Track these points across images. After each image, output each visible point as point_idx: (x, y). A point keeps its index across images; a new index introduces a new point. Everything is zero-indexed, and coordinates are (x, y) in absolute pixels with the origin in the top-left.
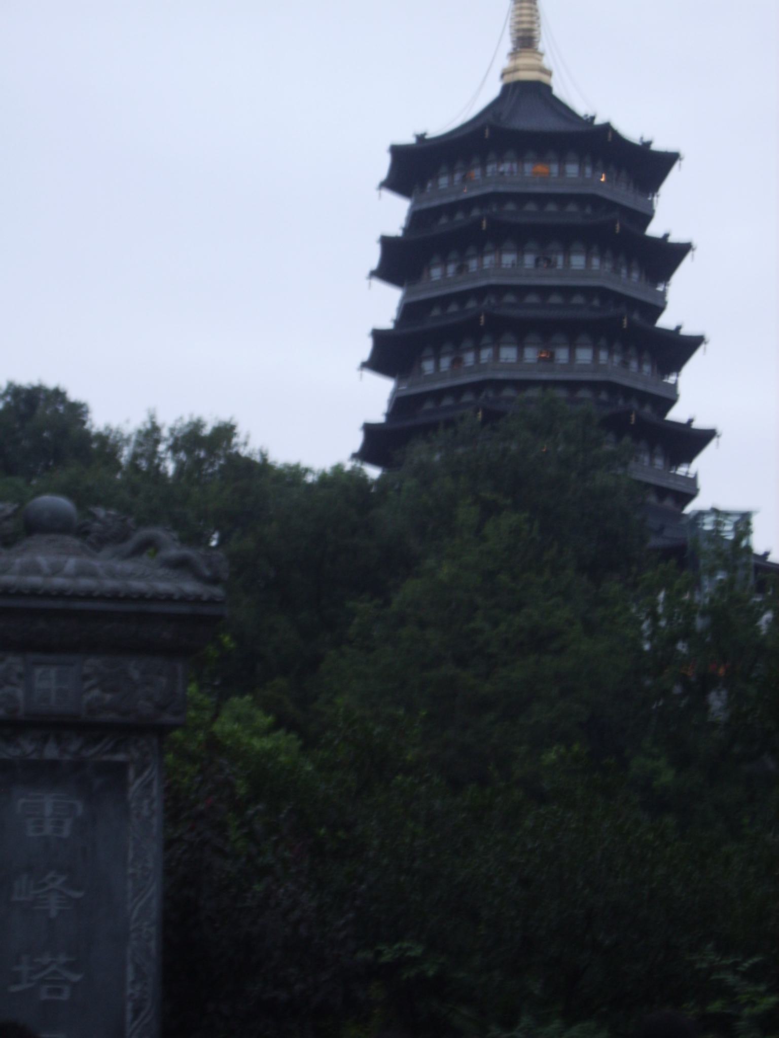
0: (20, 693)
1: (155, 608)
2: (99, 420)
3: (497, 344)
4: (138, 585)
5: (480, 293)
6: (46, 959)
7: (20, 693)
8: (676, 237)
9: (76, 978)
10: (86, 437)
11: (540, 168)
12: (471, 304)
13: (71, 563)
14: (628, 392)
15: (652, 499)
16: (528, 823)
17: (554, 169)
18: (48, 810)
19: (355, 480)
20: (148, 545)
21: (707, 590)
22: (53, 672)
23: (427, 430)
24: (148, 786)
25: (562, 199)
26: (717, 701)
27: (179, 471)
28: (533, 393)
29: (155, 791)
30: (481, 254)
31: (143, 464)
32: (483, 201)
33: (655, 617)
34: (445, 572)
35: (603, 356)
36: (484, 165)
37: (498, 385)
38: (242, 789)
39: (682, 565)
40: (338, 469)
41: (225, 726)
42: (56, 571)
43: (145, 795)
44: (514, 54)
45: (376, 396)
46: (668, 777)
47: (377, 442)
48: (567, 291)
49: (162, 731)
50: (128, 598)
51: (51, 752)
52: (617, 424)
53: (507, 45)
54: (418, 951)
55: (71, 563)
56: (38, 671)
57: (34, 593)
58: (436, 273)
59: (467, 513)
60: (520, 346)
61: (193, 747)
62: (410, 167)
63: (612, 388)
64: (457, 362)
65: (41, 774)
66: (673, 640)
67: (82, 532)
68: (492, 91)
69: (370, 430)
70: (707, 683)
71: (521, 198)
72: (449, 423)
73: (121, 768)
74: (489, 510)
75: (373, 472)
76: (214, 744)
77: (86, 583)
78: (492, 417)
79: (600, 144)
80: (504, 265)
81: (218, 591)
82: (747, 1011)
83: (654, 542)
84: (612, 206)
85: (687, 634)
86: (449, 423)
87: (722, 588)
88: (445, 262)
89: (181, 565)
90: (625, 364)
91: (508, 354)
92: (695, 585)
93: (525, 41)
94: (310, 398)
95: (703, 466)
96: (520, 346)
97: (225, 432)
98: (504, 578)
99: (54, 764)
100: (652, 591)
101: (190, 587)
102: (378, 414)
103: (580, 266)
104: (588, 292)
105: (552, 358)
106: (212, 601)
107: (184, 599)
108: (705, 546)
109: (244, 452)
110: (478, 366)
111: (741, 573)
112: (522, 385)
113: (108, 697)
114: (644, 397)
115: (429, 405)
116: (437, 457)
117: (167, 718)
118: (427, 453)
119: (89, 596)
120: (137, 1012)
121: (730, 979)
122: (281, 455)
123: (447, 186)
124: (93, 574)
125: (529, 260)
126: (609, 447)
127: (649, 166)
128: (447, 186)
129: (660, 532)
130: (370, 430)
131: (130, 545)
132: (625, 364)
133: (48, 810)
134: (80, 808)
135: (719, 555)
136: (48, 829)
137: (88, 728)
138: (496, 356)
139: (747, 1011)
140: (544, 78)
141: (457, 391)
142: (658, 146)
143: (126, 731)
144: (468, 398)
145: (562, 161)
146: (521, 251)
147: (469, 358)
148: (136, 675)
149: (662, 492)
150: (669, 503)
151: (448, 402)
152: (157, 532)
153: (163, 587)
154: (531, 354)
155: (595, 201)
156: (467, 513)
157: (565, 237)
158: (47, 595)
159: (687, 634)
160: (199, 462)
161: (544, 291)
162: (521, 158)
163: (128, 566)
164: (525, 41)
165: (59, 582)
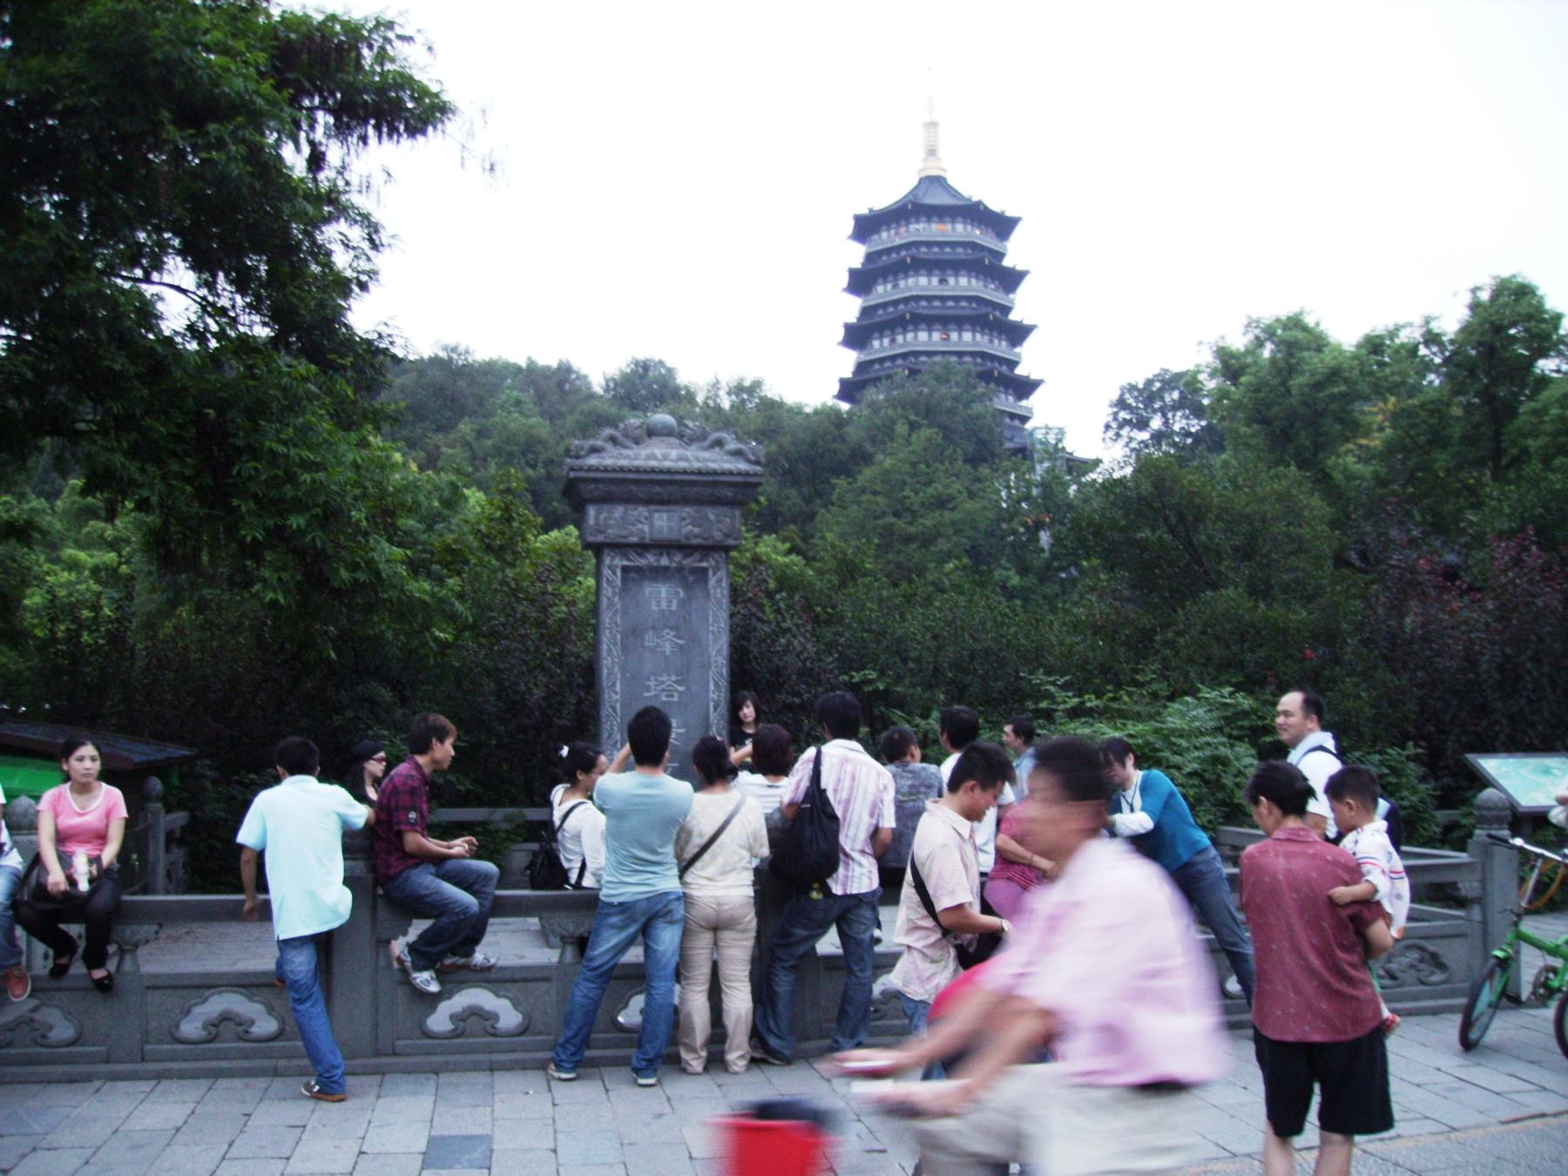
0: (646, 528)
1: (722, 478)
2: (683, 378)
3: (916, 330)
4: (713, 466)
5: (906, 300)
6: (664, 678)
7: (646, 528)
8: (1027, 322)
9: (681, 689)
10: (677, 389)
11: (941, 227)
12: (901, 307)
13: (674, 453)
14: (993, 358)
15: (1007, 420)
16: (937, 604)
17: (949, 226)
18: (664, 594)
19: (837, 412)
20: (719, 443)
21: (1041, 469)
22: (665, 516)
23: (875, 381)
24: (720, 581)
25: (953, 245)
26: (1045, 538)
27: (732, 406)
28: (937, 359)
29: (724, 584)
30: (905, 332)
31: (711, 403)
32: (908, 246)
33: (1008, 487)
34: (888, 462)
35: (978, 336)
36: (908, 223)
37: (916, 354)
38: (772, 585)
39: (1025, 458)
40: (824, 405)
41: (762, 549)
42: (665, 458)
43: (718, 586)
44: (925, 160)
45: (846, 362)
46: (1015, 580)
47: (848, 390)
48: (957, 299)
49: (727, 549)
50: (707, 473)
51: (665, 561)
52: (986, 376)
53: (922, 155)
54: (874, 675)
55: (674, 453)
56: (656, 516)
57: (653, 471)
58: (880, 289)
59: (901, 428)
60: (930, 330)
61: (744, 561)
63: (983, 355)
64: (893, 341)
65: (659, 573)
66: (1019, 502)
67: (681, 436)
69: (843, 382)
70: (1039, 526)
71: (929, 244)
72: (889, 377)
73: (704, 571)
74: (914, 426)
75: (845, 406)
76: (756, 559)
77: (683, 465)
78: (914, 372)
79: (976, 213)
80: (923, 284)
81: (758, 469)
82: (1062, 707)
83: (1008, 445)
84: (983, 248)
85: (1027, 498)
86: (889, 377)
87: (1047, 471)
88: (885, 282)
89: (737, 454)
90: (991, 341)
91: (923, 336)
92: (1032, 469)
93: (932, 152)
94: (809, 372)
95: (1034, 402)
96: (930, 330)
97: (757, 384)
98: (922, 466)
99: (666, 569)
100: (1007, 473)
101: (743, 466)
102: (848, 373)
103: (963, 284)
104: (973, 354)
105: (948, 339)
106: (755, 475)
107: (740, 474)
108: (1038, 446)
109: (769, 395)
110: (908, 288)
111: (1059, 463)
112: (930, 354)
113: (697, 530)
114: (1002, 361)
115: (877, 366)
116: (881, 397)
117: (731, 542)
118: (876, 395)
119: (685, 472)
120: (715, 708)
121: (1052, 688)
122: (790, 399)
123: (887, 238)
124: (687, 460)
125: (935, 280)
126: (980, 390)
128: (887, 238)
129: (1011, 440)
130: (843, 382)
131: (707, 442)
132: (991, 341)
133: (664, 594)
134: (682, 593)
135: (1047, 452)
136: (664, 605)
137: (686, 548)
138: (916, 337)
139: (1062, 707)
141: (893, 358)
142: (1019, 268)
143: (707, 550)
144: (899, 362)
145: (953, 222)
146: (929, 275)
147: (900, 338)
148: (712, 517)
149: (1012, 416)
150: (1017, 422)
151: (888, 364)
152: (723, 435)
153: (727, 466)
155: (973, 246)
156: (901, 428)
157: (957, 266)
158: (661, 472)
159: (1027, 498)
160: (743, 401)
161: (943, 299)
162: (929, 221)
163: (707, 455)
164: (932, 152)
165: (667, 464)
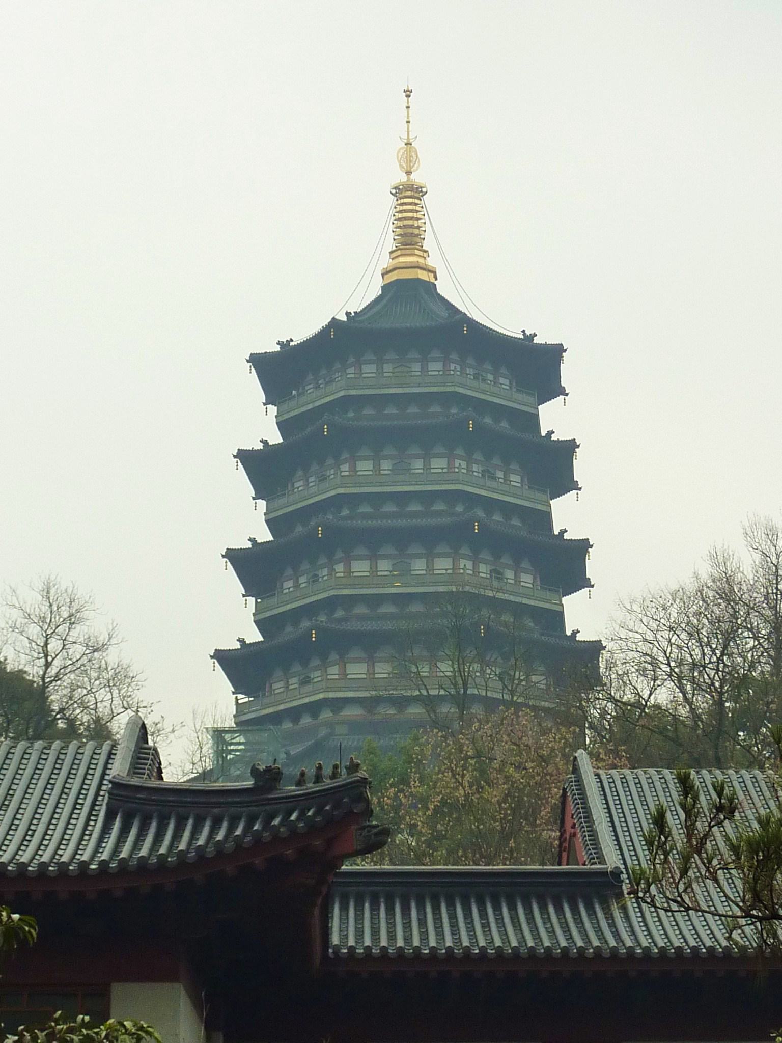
53: (390, 245)
62: (279, 371)
68: (375, 291)
93: (409, 238)
103: (442, 471)
123: (314, 397)
127: (537, 367)
128: (314, 397)
140: (423, 275)
154: (384, 567)
164: (409, 238)
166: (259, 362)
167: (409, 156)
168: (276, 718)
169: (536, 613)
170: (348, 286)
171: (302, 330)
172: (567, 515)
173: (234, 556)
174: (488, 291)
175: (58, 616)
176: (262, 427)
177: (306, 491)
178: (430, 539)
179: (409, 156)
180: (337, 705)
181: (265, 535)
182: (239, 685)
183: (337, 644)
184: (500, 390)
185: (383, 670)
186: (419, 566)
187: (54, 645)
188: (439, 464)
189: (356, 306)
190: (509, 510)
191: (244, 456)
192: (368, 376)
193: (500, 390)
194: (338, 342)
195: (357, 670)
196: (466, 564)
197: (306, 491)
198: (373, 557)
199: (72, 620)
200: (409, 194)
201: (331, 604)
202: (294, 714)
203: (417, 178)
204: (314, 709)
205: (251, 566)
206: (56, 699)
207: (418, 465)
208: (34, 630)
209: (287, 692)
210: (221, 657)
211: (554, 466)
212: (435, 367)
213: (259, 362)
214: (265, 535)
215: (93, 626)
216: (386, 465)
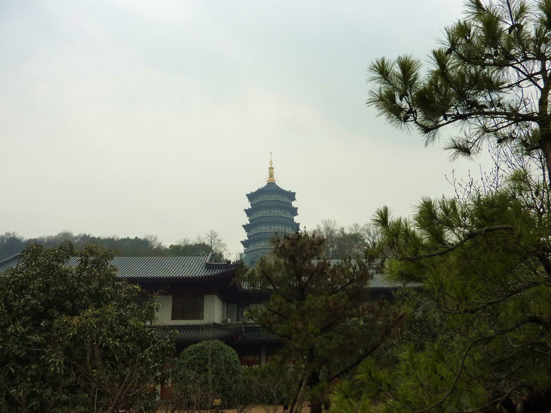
62: (251, 197)
93: (271, 176)
123: (256, 201)
127: (291, 196)
128: (256, 201)
164: (271, 176)
166: (247, 195)
167: (271, 163)
168: (250, 252)
169: (290, 219)
170: (262, 183)
171: (254, 190)
172: (294, 204)
173: (245, 210)
174: (284, 184)
175: (213, 236)
176: (248, 206)
177: (255, 216)
178: (275, 223)
179: (271, 163)
180: (260, 249)
181: (250, 207)
182: (245, 246)
183: (260, 240)
184: (286, 199)
185: (267, 227)
186: (273, 227)
187: (213, 240)
188: (276, 211)
189: (263, 186)
190: (287, 218)
191: (244, 226)
192: (265, 198)
193: (286, 199)
194: (260, 192)
195: (264, 228)
196: (280, 227)
197: (255, 216)
198: (265, 226)
199: (215, 236)
200: (271, 169)
201: (258, 234)
202: (253, 251)
203: (272, 166)
204: (256, 250)
205: (248, 212)
206: (213, 248)
207: (273, 211)
208: (209, 238)
209: (252, 247)
210: (242, 242)
211: (294, 211)
212: (275, 196)
213: (247, 195)
214: (250, 207)
215: (219, 237)
216: (267, 212)
